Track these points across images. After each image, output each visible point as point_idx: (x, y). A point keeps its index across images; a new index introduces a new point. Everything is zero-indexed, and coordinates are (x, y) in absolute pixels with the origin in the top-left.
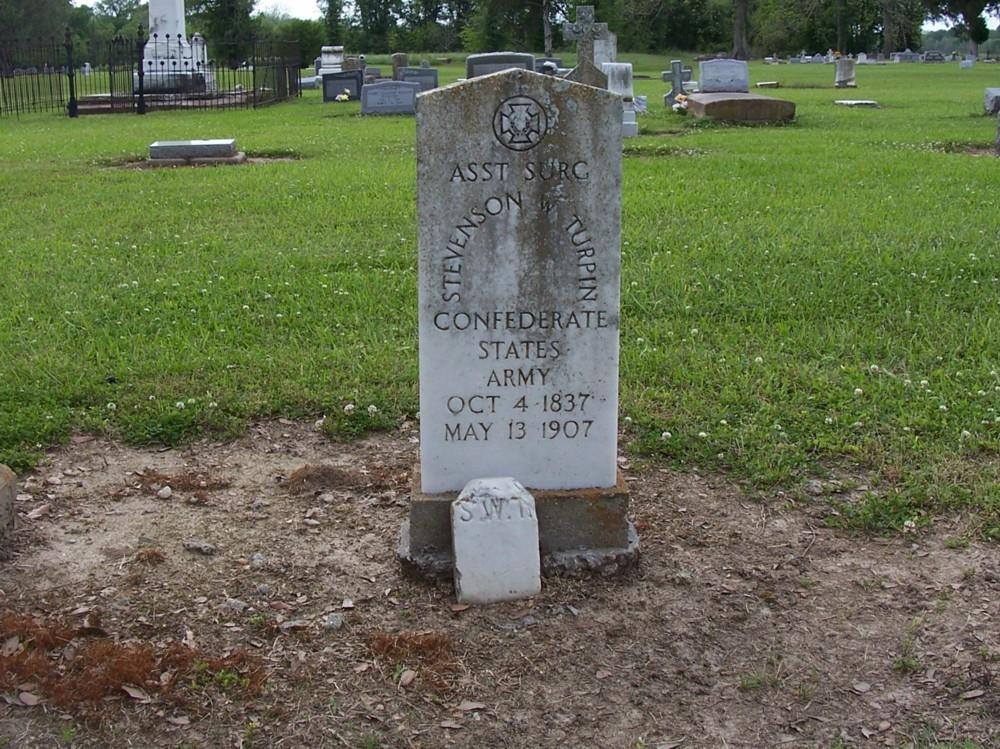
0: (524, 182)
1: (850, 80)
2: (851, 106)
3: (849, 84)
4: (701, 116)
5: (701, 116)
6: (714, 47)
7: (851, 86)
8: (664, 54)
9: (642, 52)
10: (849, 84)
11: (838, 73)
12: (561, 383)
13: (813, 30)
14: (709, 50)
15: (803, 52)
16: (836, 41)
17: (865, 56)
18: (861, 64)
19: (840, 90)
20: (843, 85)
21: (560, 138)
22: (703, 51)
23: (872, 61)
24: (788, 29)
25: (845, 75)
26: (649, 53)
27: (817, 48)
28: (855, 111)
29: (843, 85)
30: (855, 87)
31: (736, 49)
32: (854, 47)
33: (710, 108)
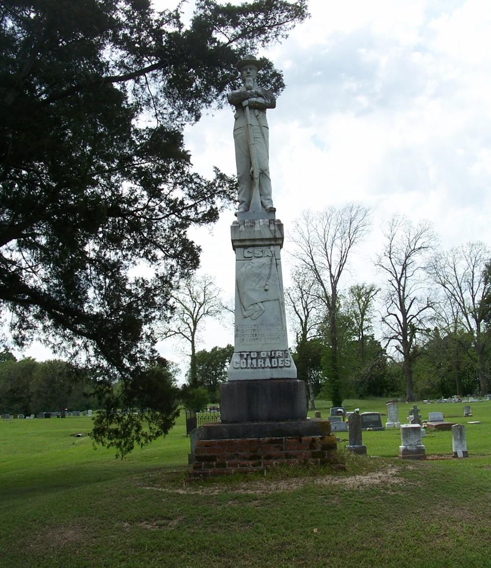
0: (459, 431)
1: (469, 413)
2: (473, 424)
3: (469, 415)
4: (434, 428)
5: (434, 428)
6: (392, 394)
7: (471, 416)
8: (368, 399)
9: (356, 398)
10: (469, 415)
11: (465, 411)
12: (463, 444)
13: (444, 383)
14: (390, 396)
15: (443, 397)
16: (456, 389)
17: (472, 398)
18: (471, 402)
19: (466, 417)
20: (467, 415)
21: (462, 428)
22: (387, 396)
23: (476, 400)
24: (431, 384)
25: (467, 412)
26: (360, 399)
27: (448, 394)
28: (471, 425)
29: (467, 415)
30: (471, 416)
31: (408, 396)
32: (467, 391)
33: (436, 426)
